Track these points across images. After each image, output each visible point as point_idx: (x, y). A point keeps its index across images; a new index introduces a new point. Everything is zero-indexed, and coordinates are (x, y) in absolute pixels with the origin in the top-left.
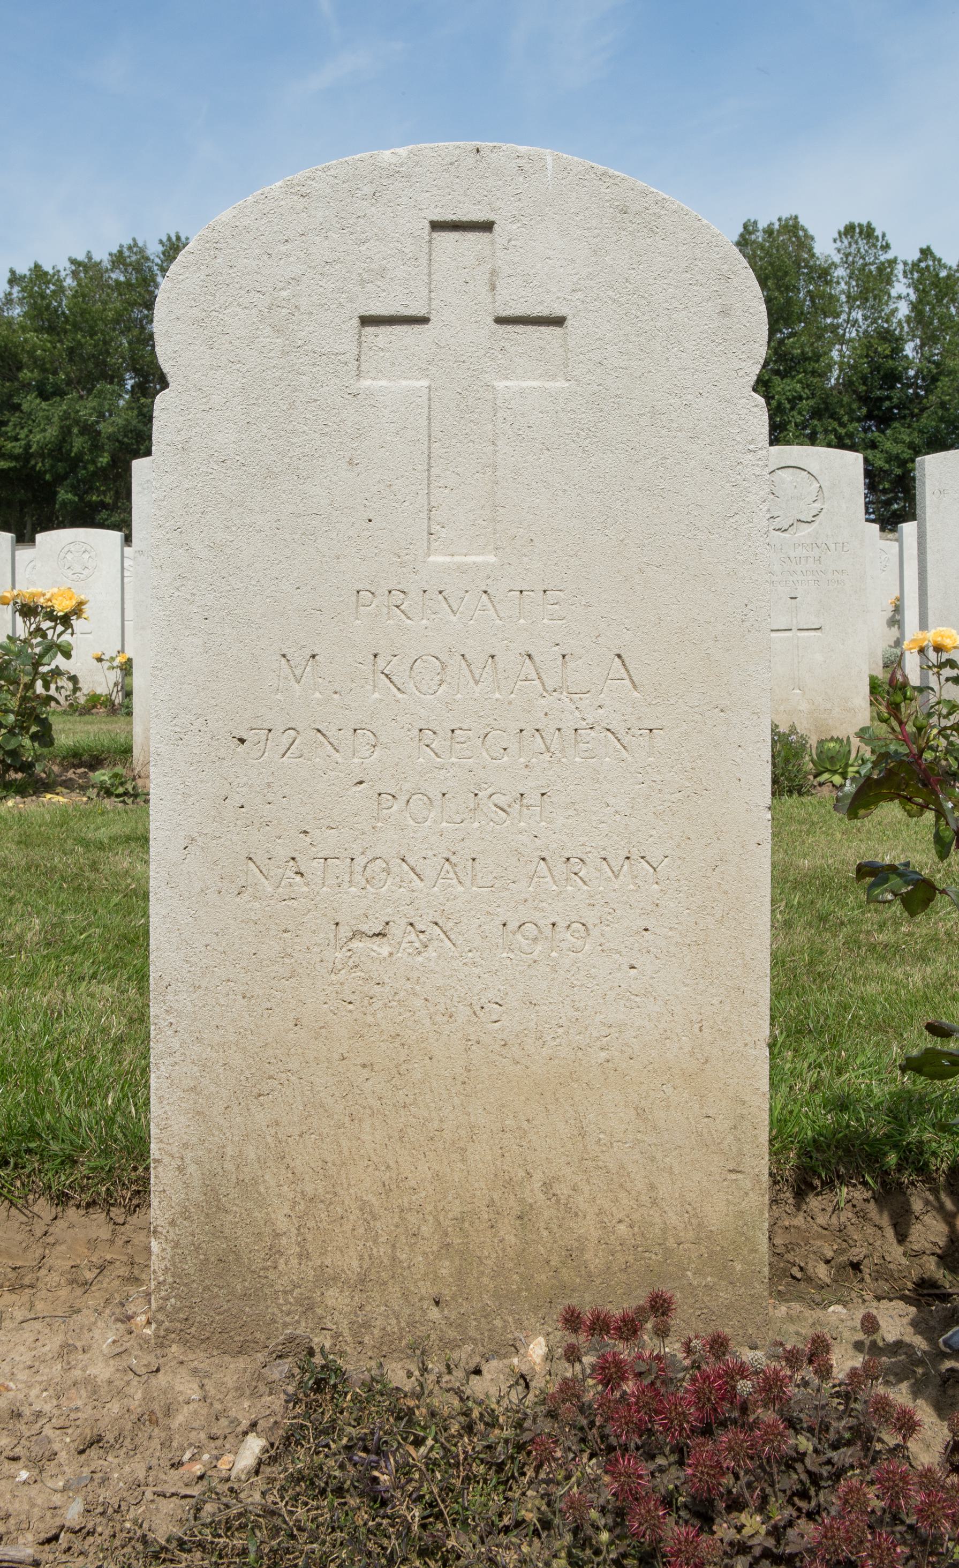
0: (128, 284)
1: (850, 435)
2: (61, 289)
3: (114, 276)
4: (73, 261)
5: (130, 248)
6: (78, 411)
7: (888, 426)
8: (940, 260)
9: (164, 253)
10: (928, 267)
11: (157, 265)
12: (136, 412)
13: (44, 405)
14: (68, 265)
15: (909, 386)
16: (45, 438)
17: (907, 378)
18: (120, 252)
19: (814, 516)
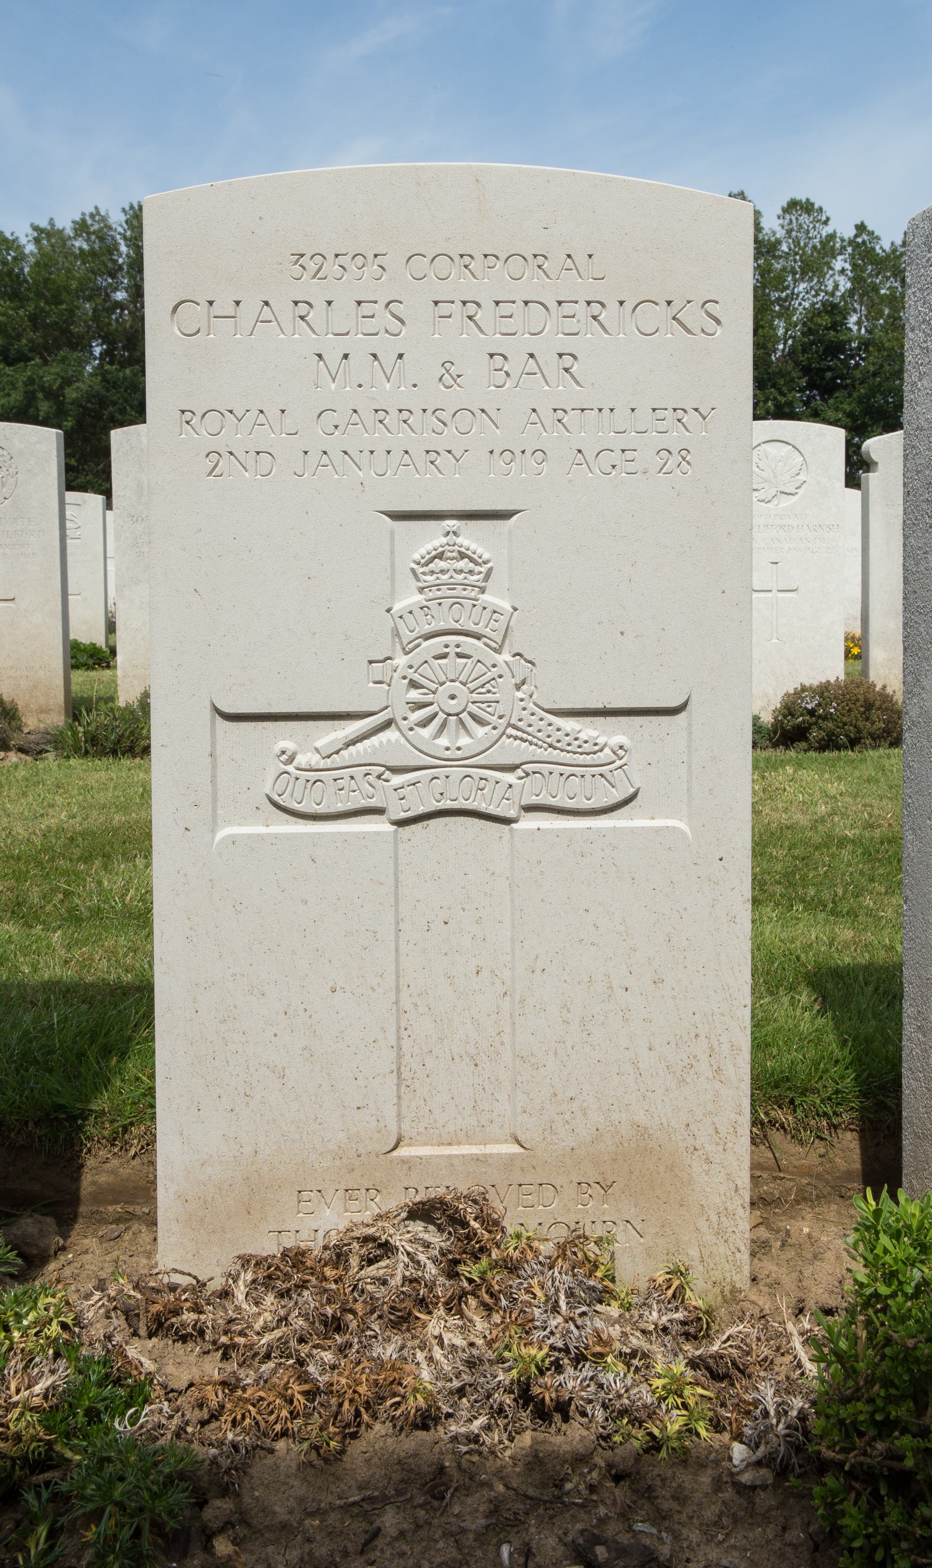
0: (93, 253)
1: (790, 404)
2: (21, 257)
3: (77, 244)
4: (36, 228)
5: (92, 216)
6: (42, 377)
7: (830, 396)
8: (873, 233)
9: (127, 222)
10: (864, 242)
11: (120, 234)
12: (99, 378)
13: (8, 370)
14: (30, 231)
15: (852, 357)
16: (9, 403)
17: (851, 350)
18: (84, 220)
19: (797, 488)
